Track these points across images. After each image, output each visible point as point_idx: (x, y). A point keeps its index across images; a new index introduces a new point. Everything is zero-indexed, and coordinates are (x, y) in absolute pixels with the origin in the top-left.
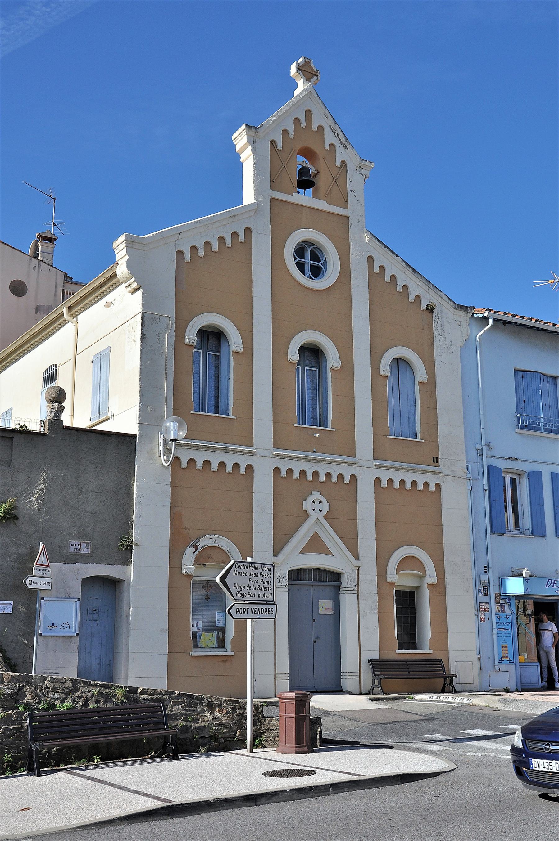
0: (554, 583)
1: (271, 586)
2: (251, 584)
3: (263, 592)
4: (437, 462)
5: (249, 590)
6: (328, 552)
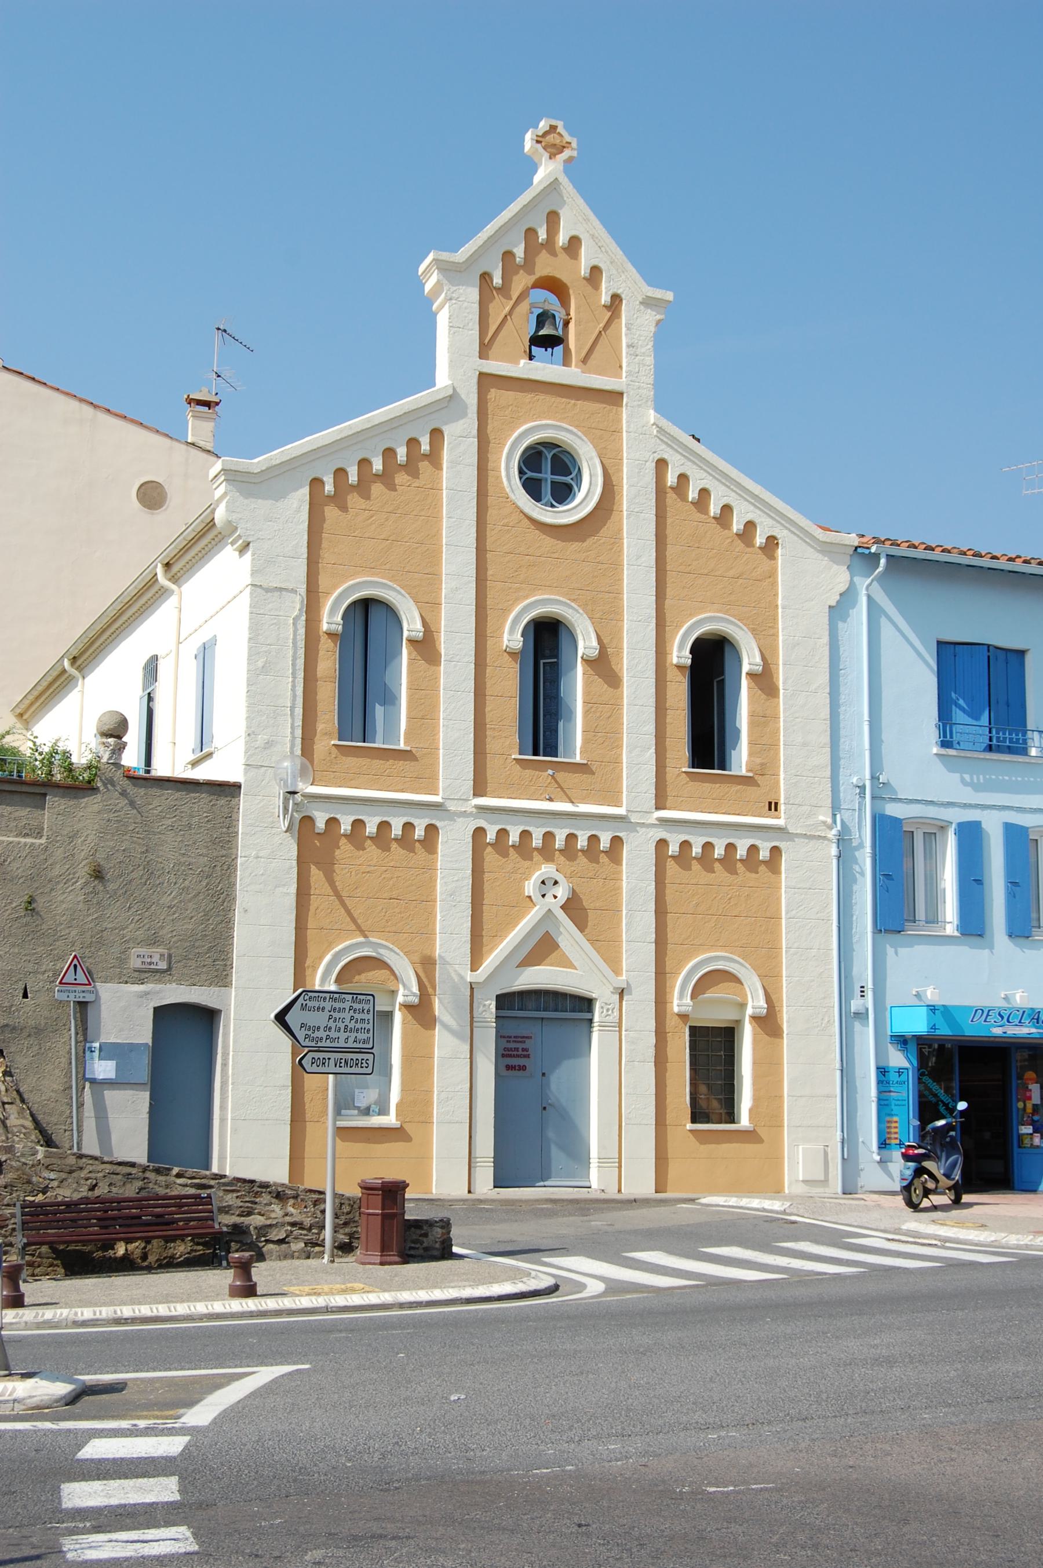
0: (988, 1015)
1: (370, 1026)
2: (331, 1024)
3: (353, 1035)
4: (776, 810)
5: (328, 1033)
6: (568, 964)
